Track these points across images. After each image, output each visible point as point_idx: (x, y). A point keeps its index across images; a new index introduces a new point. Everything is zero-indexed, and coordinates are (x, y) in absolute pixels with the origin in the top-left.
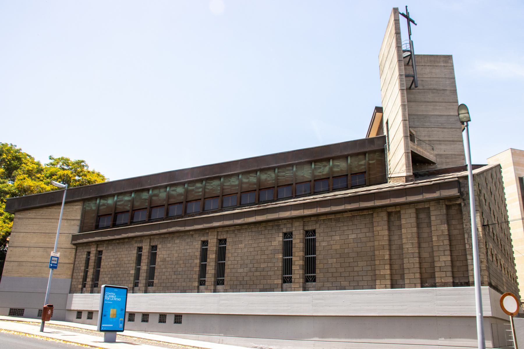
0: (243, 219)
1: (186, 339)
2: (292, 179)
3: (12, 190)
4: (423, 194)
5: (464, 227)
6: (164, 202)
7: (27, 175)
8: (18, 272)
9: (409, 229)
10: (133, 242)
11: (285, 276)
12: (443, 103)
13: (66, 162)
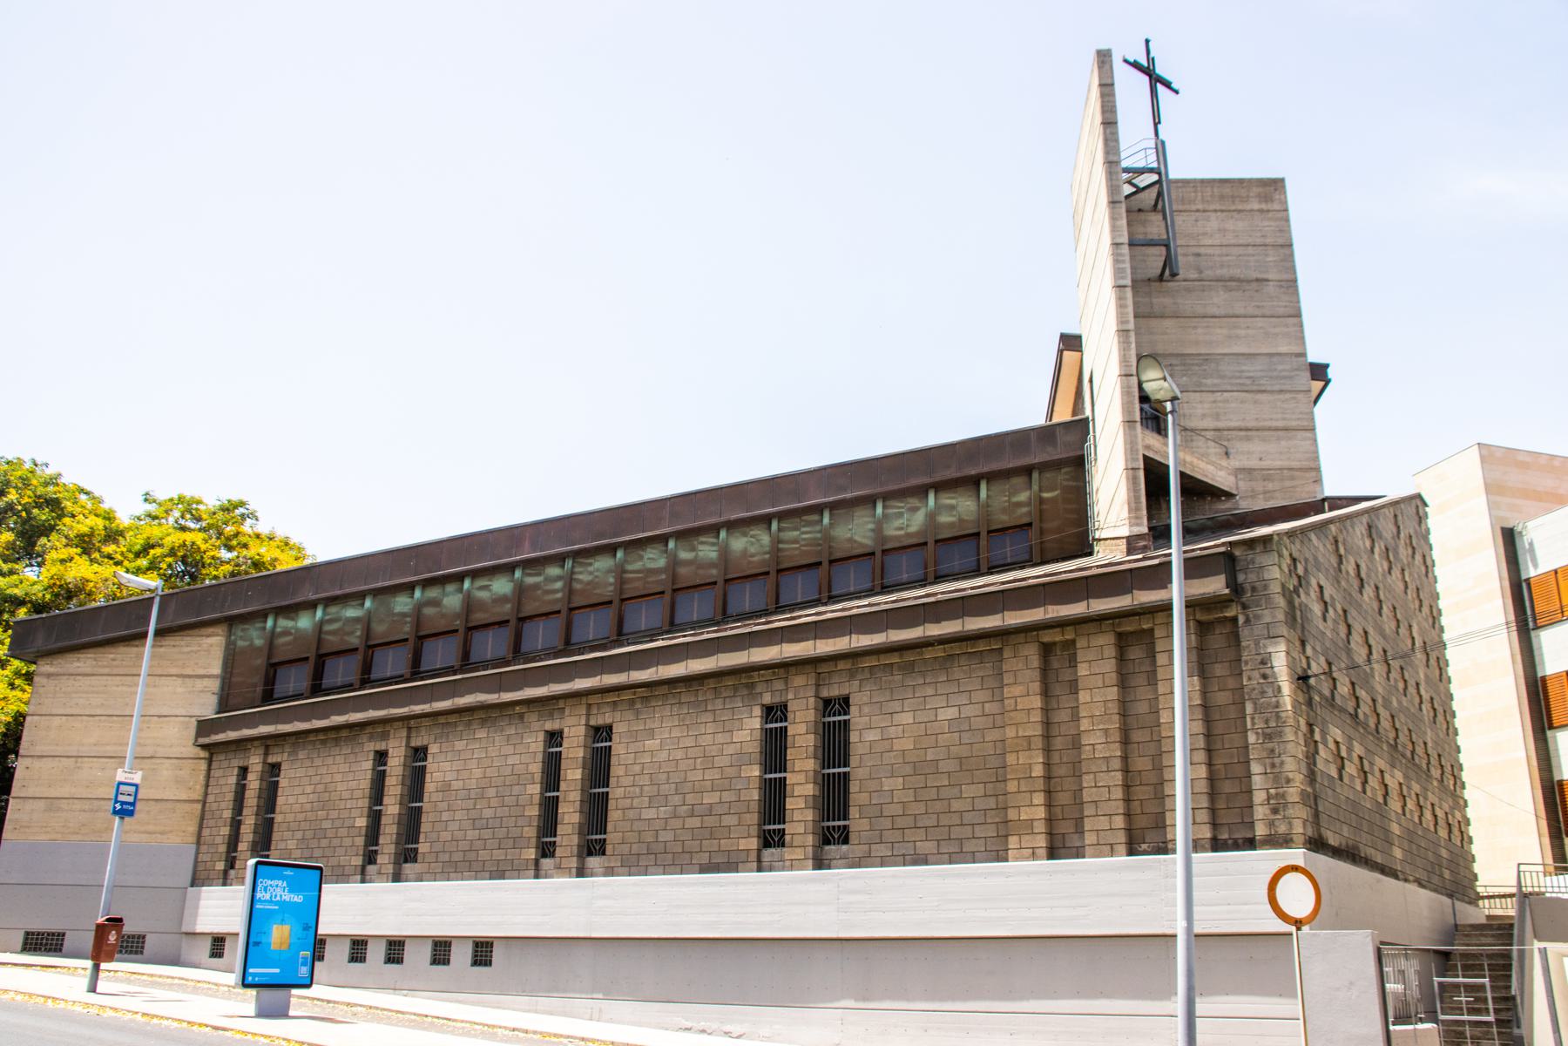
0: (655, 669)
1: (504, 1009)
2: (820, 548)
3: (34, 594)
4: (1134, 591)
5: (1245, 683)
6: (458, 622)
7: (79, 550)
8: (49, 829)
9: (1097, 690)
10: (364, 738)
11: (826, 824)
12: (1258, 319)
13: (189, 507)
